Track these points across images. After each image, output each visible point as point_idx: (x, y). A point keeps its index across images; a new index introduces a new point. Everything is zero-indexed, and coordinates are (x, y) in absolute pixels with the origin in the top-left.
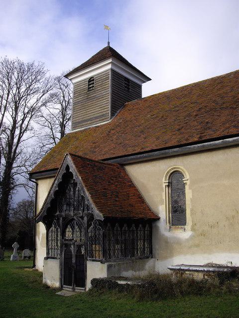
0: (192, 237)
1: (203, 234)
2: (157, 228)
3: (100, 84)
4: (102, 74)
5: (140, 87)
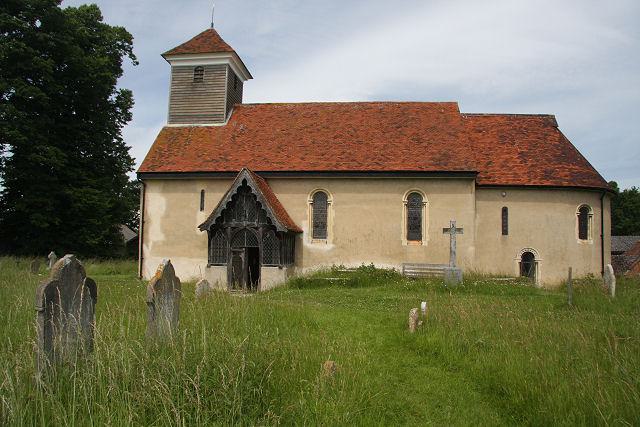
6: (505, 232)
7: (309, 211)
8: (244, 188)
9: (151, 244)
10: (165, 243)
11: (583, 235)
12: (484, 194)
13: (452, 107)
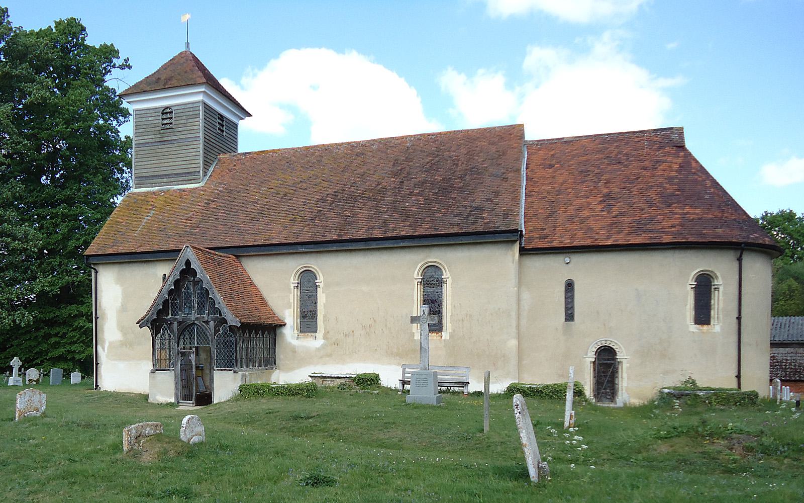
0: (323, 347)
1: (336, 343)
2: (282, 335)
3: (181, 122)
4: (188, 106)
5: (235, 126)
6: (570, 316)
7: (293, 296)
8: (188, 271)
9: (107, 345)
10: (123, 344)
11: (703, 315)
12: (537, 263)
13: (385, 67)
